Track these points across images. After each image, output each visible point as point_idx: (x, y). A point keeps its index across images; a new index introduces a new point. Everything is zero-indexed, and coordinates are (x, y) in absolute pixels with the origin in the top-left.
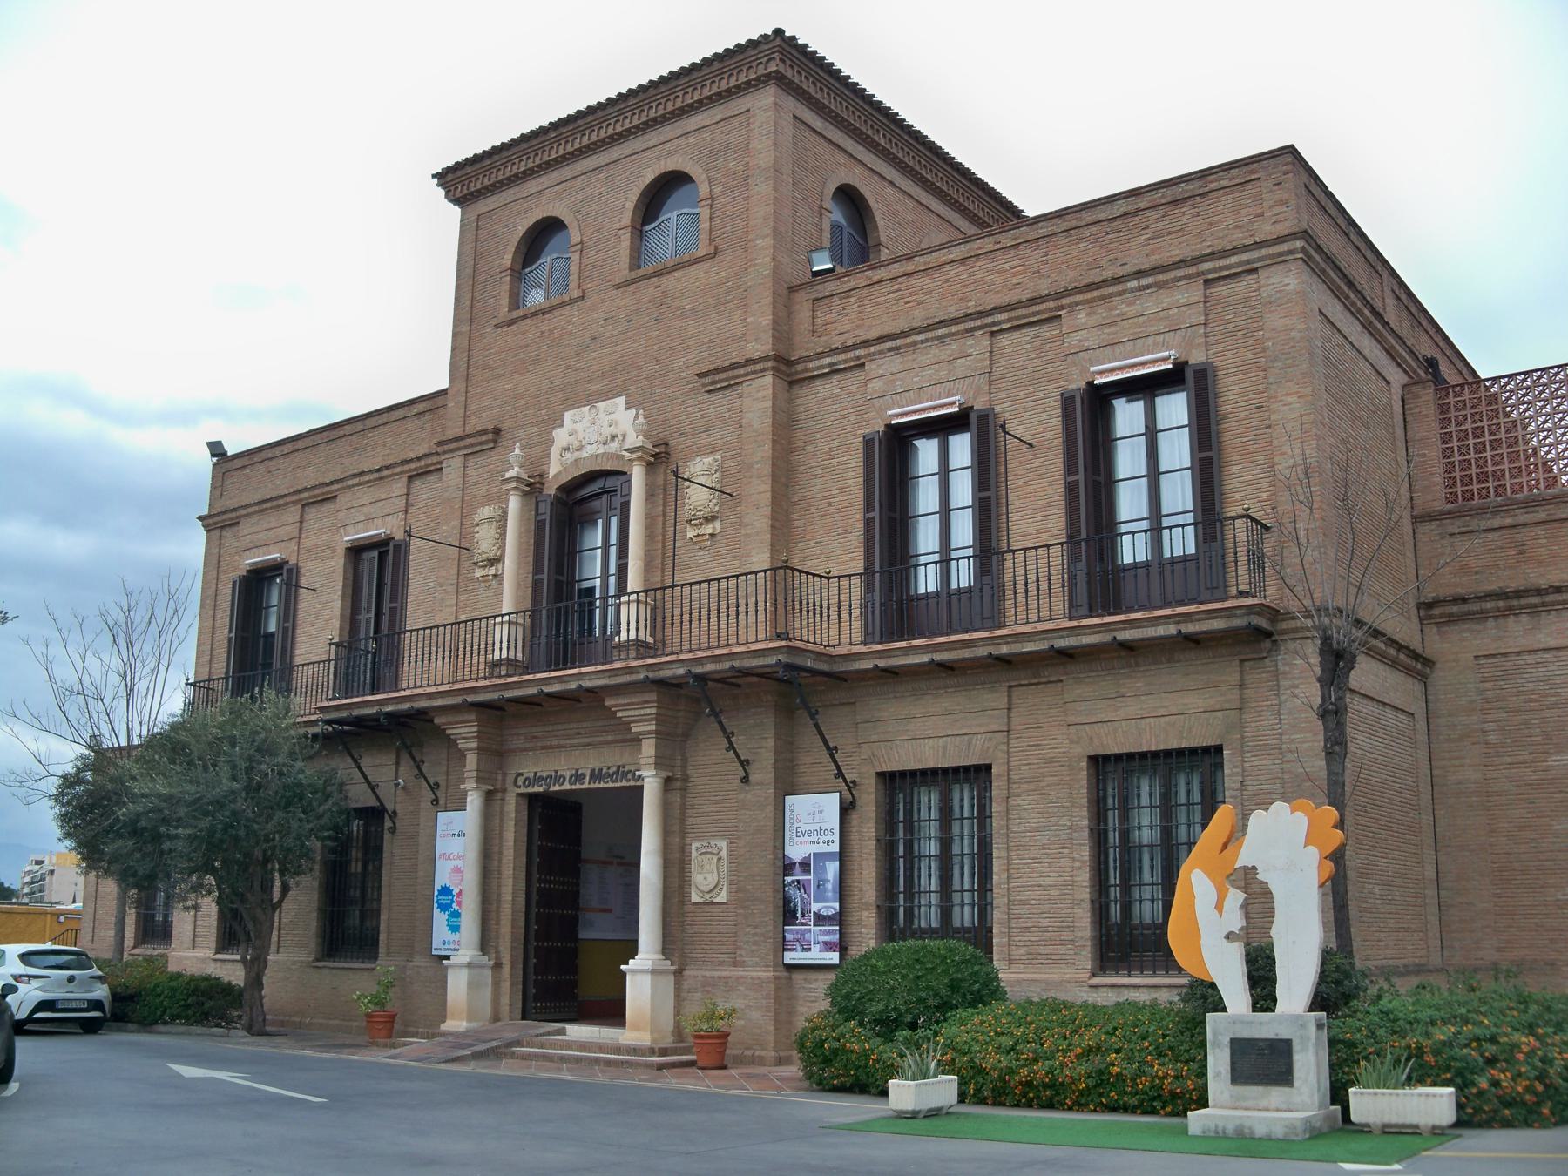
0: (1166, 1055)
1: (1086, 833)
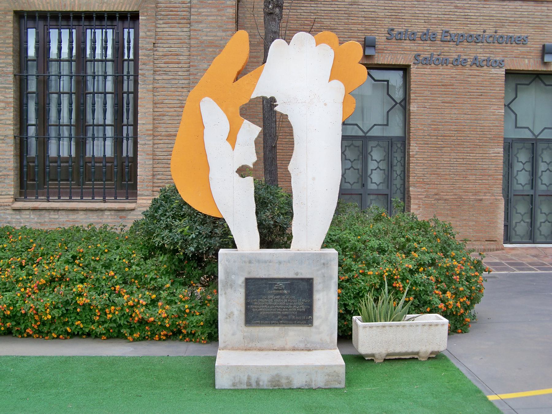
0: (132, 284)
1: (11, 78)
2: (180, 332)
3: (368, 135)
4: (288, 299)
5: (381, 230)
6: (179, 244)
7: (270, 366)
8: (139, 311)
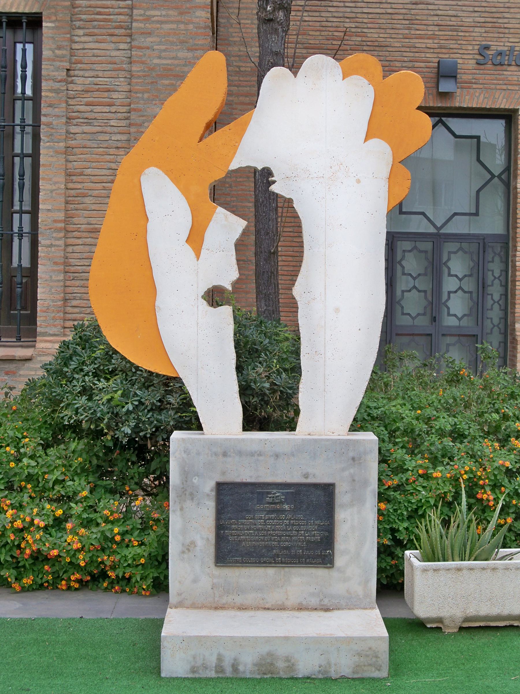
0: (22, 489)
2: (104, 575)
3: (442, 231)
4: (290, 519)
5: (458, 399)
6: (105, 422)
7: (256, 638)
8: (32, 538)
